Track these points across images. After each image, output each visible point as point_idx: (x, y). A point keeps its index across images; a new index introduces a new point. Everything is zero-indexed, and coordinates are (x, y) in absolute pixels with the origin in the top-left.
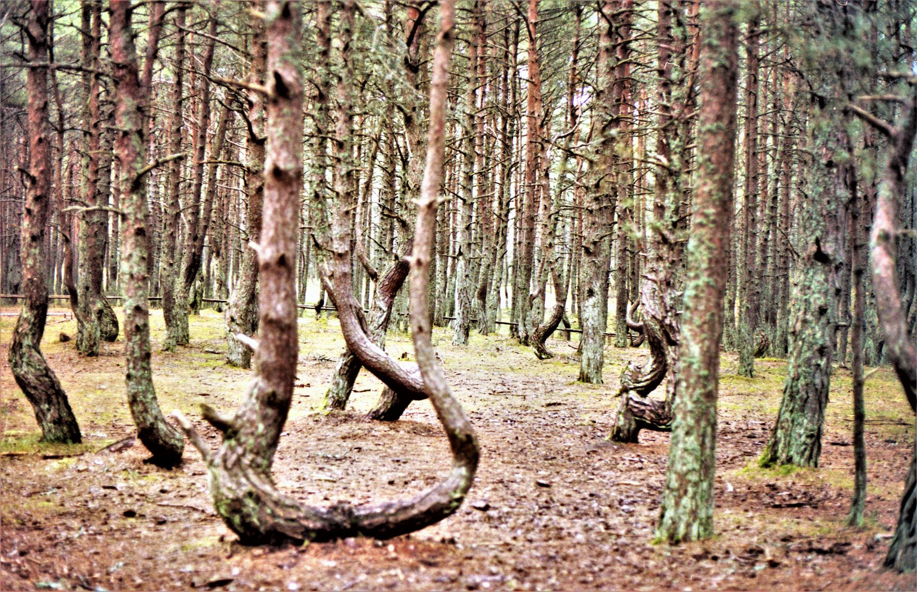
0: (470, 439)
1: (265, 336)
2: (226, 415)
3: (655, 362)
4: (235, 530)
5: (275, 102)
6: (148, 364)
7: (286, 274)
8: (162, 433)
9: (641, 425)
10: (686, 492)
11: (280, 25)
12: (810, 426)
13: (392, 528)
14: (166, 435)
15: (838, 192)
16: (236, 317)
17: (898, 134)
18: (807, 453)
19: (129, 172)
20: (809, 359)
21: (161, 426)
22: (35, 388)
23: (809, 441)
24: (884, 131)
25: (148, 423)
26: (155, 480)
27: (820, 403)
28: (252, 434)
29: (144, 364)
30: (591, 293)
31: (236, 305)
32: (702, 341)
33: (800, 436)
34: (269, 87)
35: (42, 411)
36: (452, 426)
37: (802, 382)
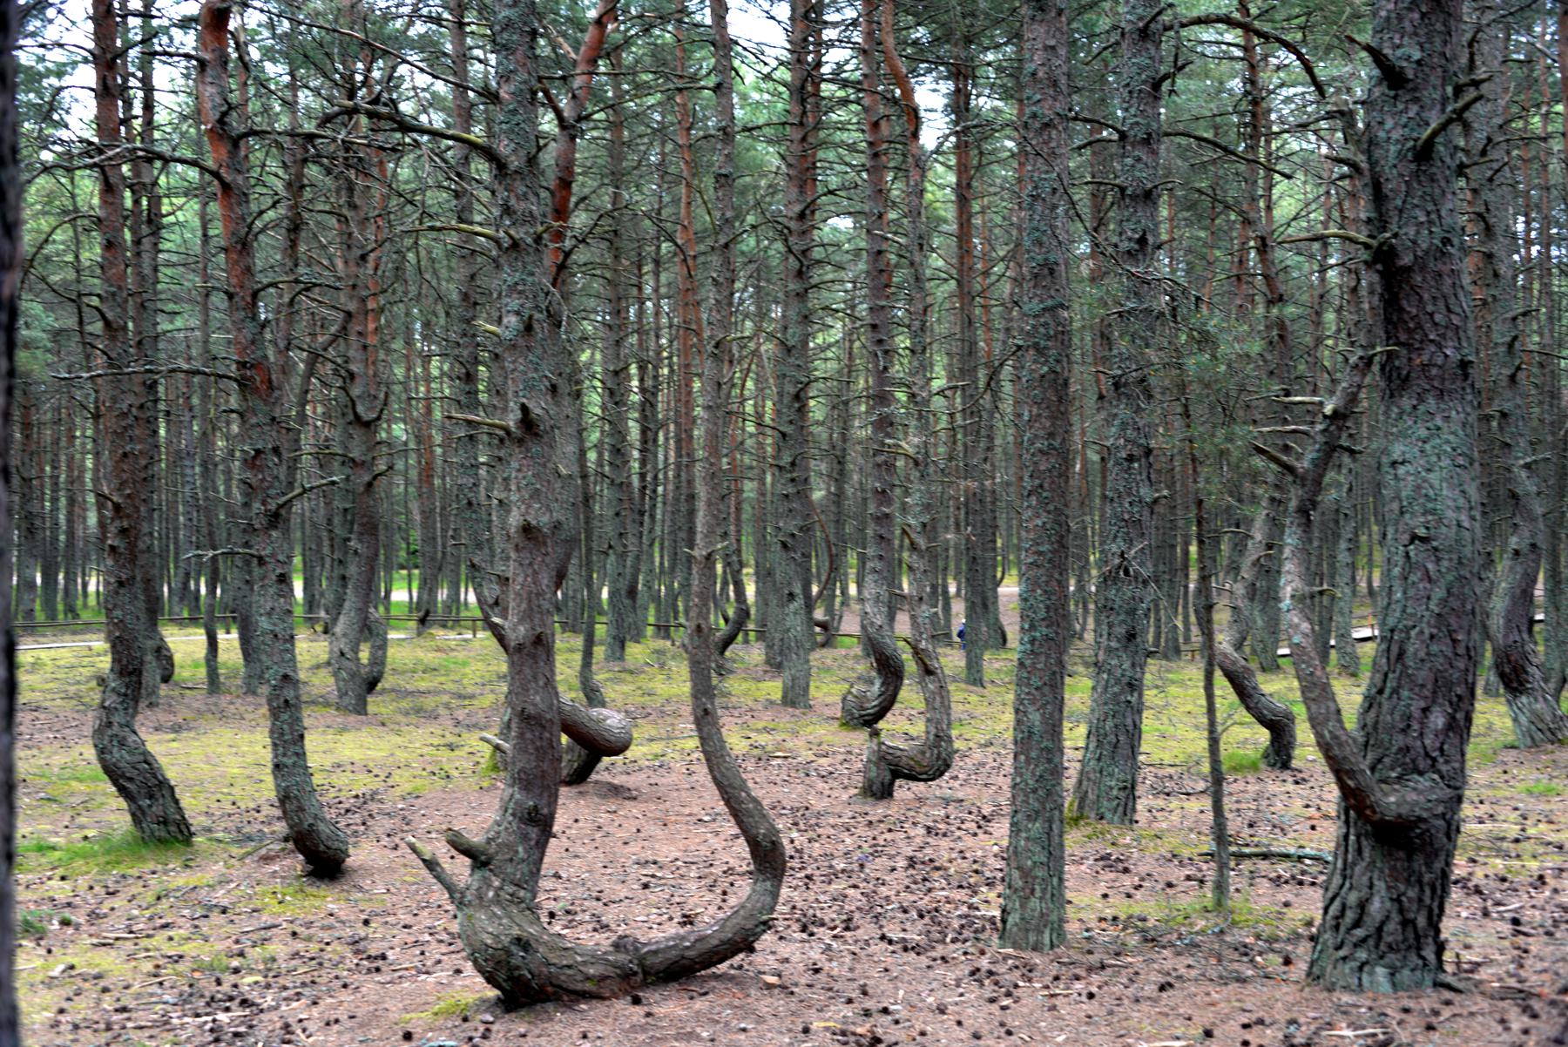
0: (776, 846)
1: (521, 735)
2: (476, 838)
3: (883, 684)
4: (497, 985)
5: (521, 441)
6: (302, 747)
7: (544, 657)
8: (323, 837)
9: (897, 774)
10: (1033, 891)
11: (521, 341)
12: (1122, 776)
13: (681, 969)
14: (329, 838)
15: (1142, 491)
16: (346, 650)
17: (1307, 471)
18: (1121, 809)
19: (264, 503)
20: (1115, 695)
21: (321, 826)
22: (130, 779)
23: (1122, 794)
24: (1290, 469)
25: (306, 825)
26: (329, 900)
27: (1132, 747)
28: (511, 860)
29: (297, 749)
30: (791, 596)
31: (345, 635)
32: (1043, 706)
33: (1111, 788)
34: (512, 420)
35: (140, 807)
36: (754, 831)
37: (1110, 724)
